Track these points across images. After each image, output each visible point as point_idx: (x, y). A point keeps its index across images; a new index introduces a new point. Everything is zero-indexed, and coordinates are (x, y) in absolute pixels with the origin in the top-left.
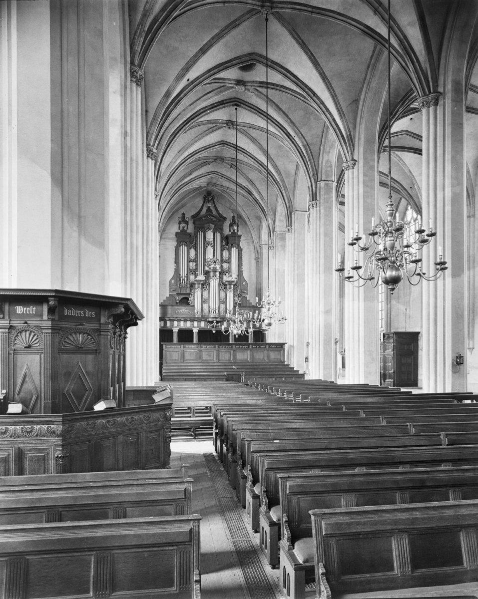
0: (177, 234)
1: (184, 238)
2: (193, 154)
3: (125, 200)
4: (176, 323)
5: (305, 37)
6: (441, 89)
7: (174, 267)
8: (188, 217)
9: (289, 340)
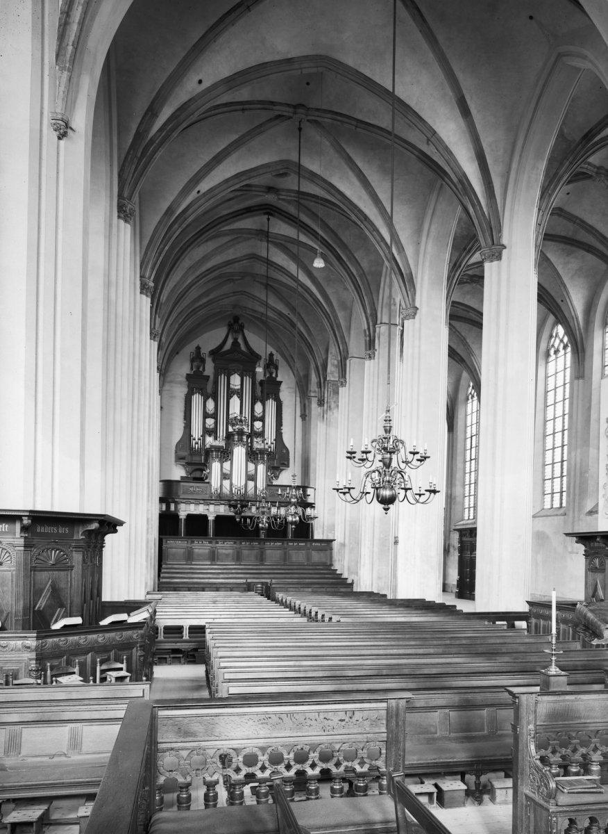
0: (188, 377)
1: (198, 383)
2: (210, 271)
3: (107, 369)
8: (205, 350)
9: (339, 537)
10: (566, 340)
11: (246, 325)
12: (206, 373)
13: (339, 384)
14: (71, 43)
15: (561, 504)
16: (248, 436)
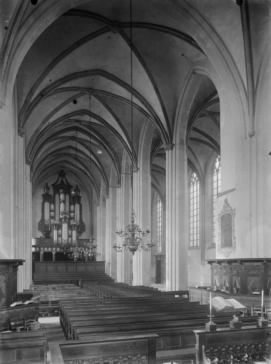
1: (47, 198)
5: (110, 106)
6: (174, 143)
8: (49, 185)
10: (197, 178)
11: (66, 174)
12: (50, 194)
13: (106, 198)
14: (4, 71)
15: (197, 244)
16: (68, 220)
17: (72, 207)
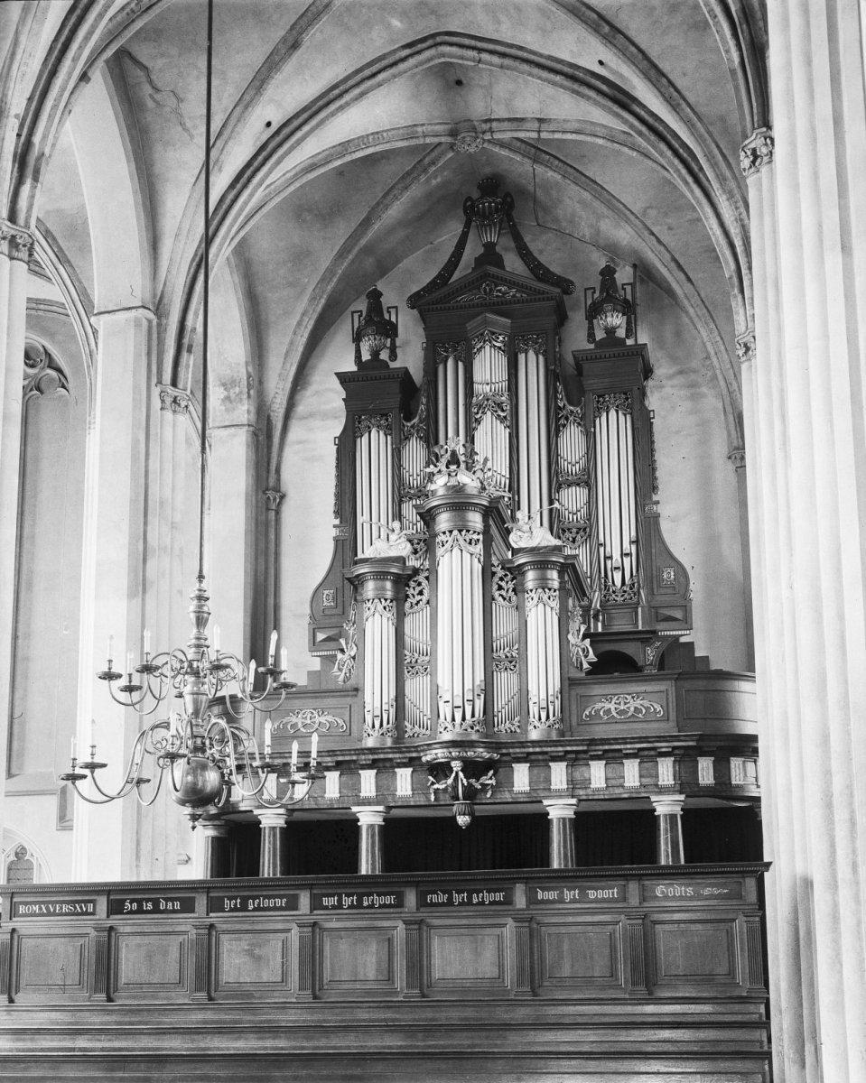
1: (390, 402)
4: (368, 780)
7: (334, 532)
8: (393, 296)
17: (572, 444)
